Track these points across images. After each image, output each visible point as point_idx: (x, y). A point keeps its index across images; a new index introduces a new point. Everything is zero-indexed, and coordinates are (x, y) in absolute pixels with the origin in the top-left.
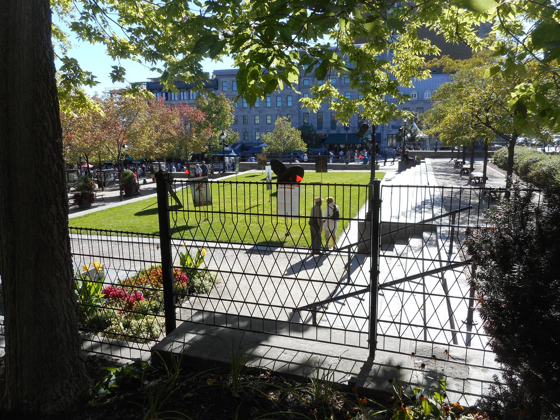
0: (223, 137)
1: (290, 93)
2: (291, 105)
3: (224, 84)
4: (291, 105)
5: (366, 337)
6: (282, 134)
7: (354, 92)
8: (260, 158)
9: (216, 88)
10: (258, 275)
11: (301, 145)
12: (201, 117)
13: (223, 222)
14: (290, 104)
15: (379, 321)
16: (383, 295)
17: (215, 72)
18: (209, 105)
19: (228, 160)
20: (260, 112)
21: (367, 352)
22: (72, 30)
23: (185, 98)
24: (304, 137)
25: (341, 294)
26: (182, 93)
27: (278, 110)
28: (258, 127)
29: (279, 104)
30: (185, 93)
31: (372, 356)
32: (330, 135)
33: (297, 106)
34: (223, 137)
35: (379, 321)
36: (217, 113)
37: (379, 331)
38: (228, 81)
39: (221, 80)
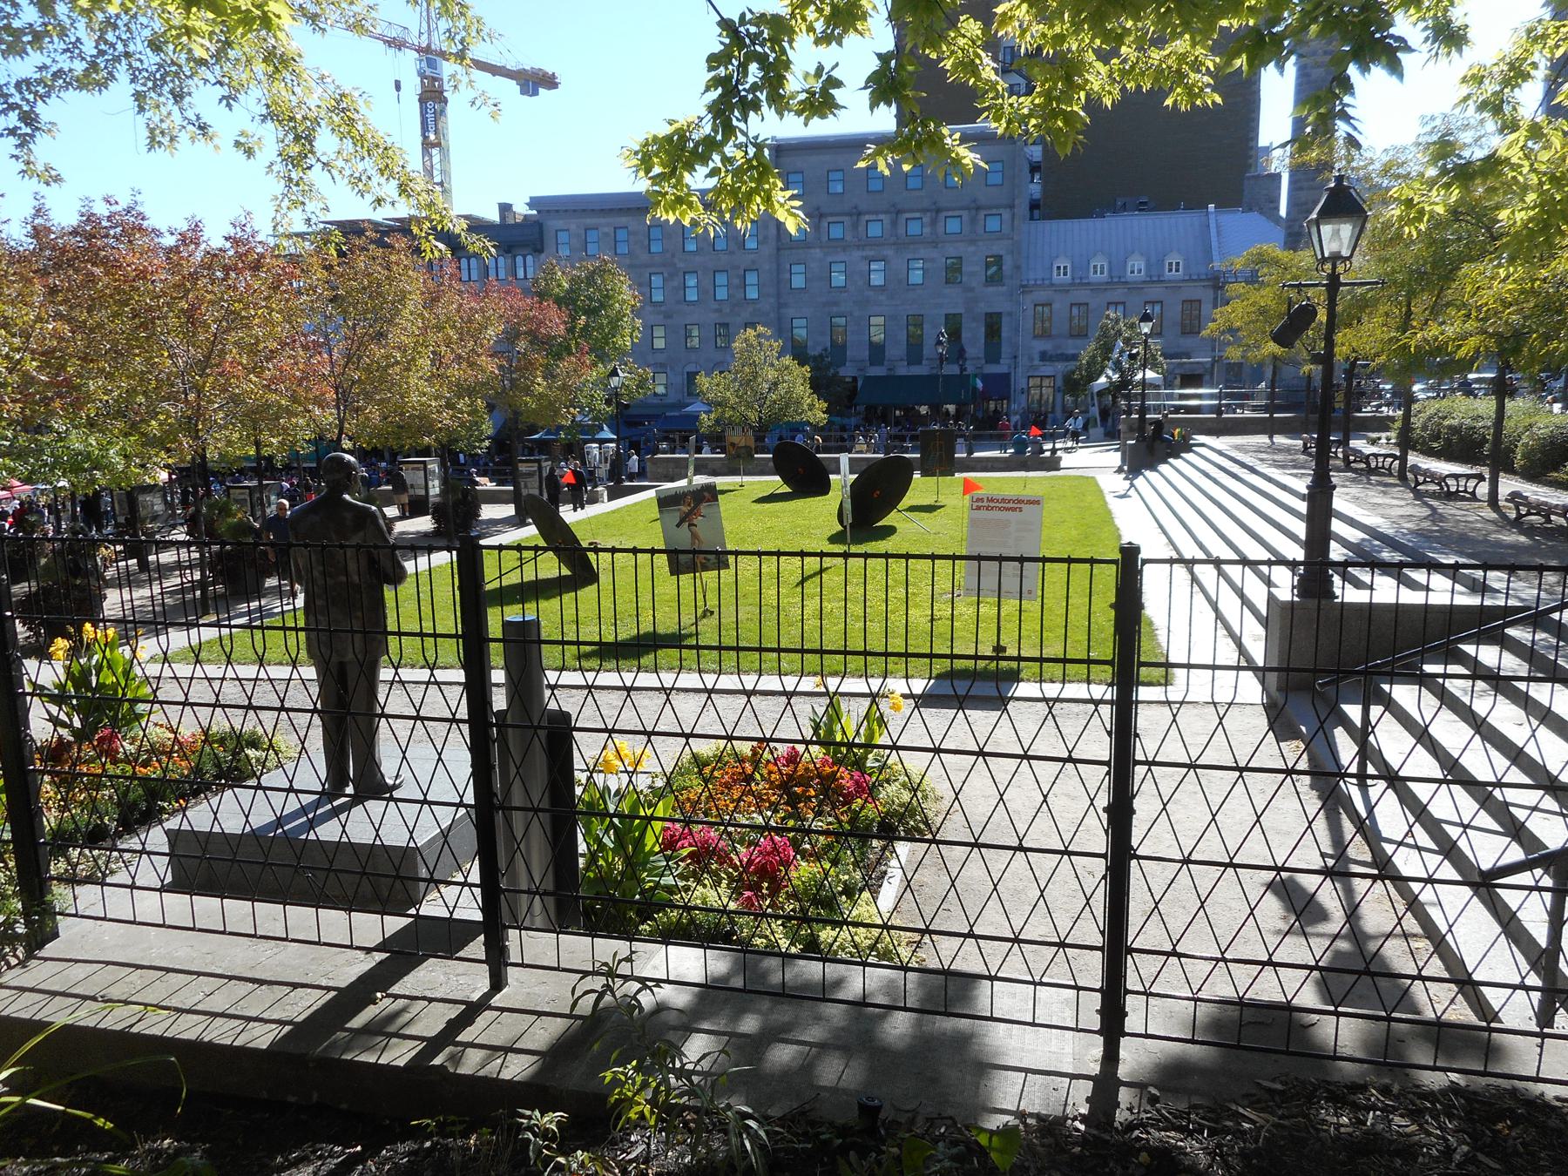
0: (614, 382)
1: (753, 262)
2: (755, 296)
3: (563, 237)
4: (755, 296)
5: (1096, 1000)
6: (755, 375)
7: (933, 260)
8: (736, 440)
9: (538, 249)
10: (430, 803)
11: (811, 407)
12: (555, 323)
13: (228, 650)
14: (752, 294)
15: (1131, 951)
16: (1323, 855)
17: (534, 202)
18: (571, 290)
19: (596, 452)
20: (668, 316)
21: (1095, 1048)
22: (1460, 51)
23: (474, 276)
24: (817, 385)
25: (1521, 814)
26: (519, 259)
27: (719, 311)
28: (661, 358)
29: (722, 294)
30: (529, 259)
31: (1111, 1056)
32: (868, 379)
33: (772, 300)
34: (614, 382)
35: (1131, 951)
36: (591, 312)
37: (1132, 982)
38: (573, 227)
39: (553, 224)
